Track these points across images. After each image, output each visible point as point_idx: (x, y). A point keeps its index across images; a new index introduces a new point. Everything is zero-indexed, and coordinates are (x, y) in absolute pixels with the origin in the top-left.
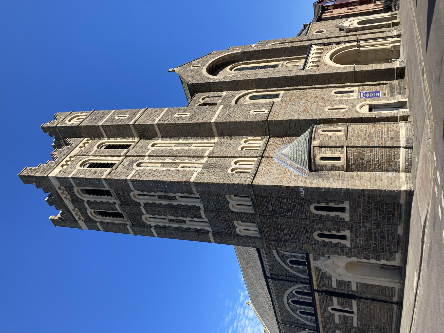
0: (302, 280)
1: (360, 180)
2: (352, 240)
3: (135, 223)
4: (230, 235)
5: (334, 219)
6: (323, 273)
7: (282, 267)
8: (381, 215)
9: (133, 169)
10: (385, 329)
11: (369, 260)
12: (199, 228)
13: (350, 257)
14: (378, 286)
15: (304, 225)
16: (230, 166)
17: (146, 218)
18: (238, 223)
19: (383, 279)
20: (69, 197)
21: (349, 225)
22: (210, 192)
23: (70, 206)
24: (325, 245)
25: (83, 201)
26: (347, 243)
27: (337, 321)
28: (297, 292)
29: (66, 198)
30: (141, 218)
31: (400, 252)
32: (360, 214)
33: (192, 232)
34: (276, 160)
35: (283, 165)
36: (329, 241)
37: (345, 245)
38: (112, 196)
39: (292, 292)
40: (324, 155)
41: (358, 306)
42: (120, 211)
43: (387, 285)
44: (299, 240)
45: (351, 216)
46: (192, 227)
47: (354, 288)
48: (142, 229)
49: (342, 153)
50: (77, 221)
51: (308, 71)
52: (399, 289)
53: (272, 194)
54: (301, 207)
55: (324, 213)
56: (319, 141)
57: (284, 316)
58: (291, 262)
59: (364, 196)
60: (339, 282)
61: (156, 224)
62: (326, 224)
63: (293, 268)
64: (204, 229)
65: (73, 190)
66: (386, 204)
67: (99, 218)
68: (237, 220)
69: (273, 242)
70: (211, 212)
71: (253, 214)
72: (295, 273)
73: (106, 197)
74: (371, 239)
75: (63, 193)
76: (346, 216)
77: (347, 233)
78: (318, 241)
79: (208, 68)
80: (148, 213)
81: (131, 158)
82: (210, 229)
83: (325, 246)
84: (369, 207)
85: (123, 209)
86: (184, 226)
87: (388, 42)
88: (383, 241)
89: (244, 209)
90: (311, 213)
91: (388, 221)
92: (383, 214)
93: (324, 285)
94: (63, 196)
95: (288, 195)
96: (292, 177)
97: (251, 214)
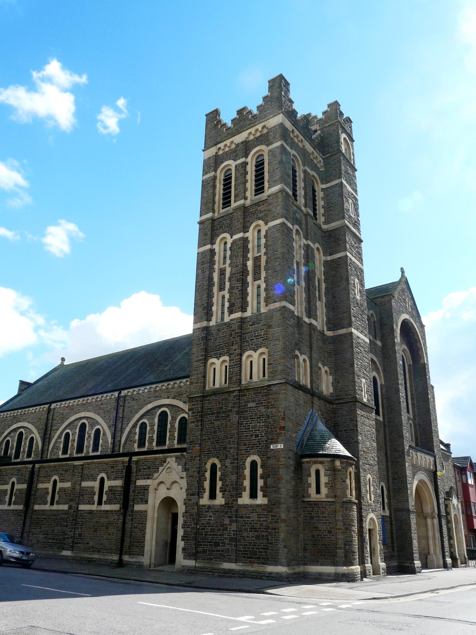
0: (119, 439)
1: (294, 517)
2: (209, 507)
3: (216, 223)
4: (206, 350)
6: (158, 468)
7: (137, 412)
8: (248, 543)
9: (293, 225)
10: (79, 545)
11: (182, 528)
12: (214, 308)
14: (144, 537)
15: (229, 446)
16: (301, 354)
17: (224, 238)
18: (224, 361)
20: (252, 137)
21: (232, 504)
22: (270, 327)
23: (239, 139)
24: (201, 472)
26: (205, 500)
27: (85, 484)
28: (98, 431)
30: (225, 232)
31: (197, 565)
32: (249, 517)
33: (208, 300)
34: (310, 413)
35: (305, 421)
36: (206, 478)
39: (98, 423)
40: (322, 473)
41: (111, 511)
42: (234, 205)
43: (147, 548)
44: (205, 440)
45: (245, 506)
46: (214, 300)
47: (138, 507)
48: (209, 233)
49: (327, 496)
50: (216, 145)
52: (143, 563)
53: (271, 408)
54: (254, 444)
55: (247, 472)
57: (61, 412)
58: (144, 424)
59: (276, 522)
60: (146, 488)
61: (217, 251)
62: (232, 474)
63: (134, 426)
64: (212, 316)
65: (262, 144)
66: (266, 549)
67: (220, 176)
68: (230, 361)
69: (200, 406)
70: (241, 327)
72: (128, 429)
73: (254, 188)
74: (212, 530)
75: (257, 130)
76: (245, 499)
77: (220, 500)
78: (206, 464)
79: (406, 321)
80: (233, 243)
81: (304, 222)
82: (213, 323)
83: (199, 472)
84: (259, 528)
85: (236, 209)
86: (215, 289)
88: (210, 545)
90: (247, 457)
91: (240, 551)
92: (250, 545)
93: (140, 470)
94: (252, 130)
95: (271, 428)
96: (295, 433)
97: (240, 380)
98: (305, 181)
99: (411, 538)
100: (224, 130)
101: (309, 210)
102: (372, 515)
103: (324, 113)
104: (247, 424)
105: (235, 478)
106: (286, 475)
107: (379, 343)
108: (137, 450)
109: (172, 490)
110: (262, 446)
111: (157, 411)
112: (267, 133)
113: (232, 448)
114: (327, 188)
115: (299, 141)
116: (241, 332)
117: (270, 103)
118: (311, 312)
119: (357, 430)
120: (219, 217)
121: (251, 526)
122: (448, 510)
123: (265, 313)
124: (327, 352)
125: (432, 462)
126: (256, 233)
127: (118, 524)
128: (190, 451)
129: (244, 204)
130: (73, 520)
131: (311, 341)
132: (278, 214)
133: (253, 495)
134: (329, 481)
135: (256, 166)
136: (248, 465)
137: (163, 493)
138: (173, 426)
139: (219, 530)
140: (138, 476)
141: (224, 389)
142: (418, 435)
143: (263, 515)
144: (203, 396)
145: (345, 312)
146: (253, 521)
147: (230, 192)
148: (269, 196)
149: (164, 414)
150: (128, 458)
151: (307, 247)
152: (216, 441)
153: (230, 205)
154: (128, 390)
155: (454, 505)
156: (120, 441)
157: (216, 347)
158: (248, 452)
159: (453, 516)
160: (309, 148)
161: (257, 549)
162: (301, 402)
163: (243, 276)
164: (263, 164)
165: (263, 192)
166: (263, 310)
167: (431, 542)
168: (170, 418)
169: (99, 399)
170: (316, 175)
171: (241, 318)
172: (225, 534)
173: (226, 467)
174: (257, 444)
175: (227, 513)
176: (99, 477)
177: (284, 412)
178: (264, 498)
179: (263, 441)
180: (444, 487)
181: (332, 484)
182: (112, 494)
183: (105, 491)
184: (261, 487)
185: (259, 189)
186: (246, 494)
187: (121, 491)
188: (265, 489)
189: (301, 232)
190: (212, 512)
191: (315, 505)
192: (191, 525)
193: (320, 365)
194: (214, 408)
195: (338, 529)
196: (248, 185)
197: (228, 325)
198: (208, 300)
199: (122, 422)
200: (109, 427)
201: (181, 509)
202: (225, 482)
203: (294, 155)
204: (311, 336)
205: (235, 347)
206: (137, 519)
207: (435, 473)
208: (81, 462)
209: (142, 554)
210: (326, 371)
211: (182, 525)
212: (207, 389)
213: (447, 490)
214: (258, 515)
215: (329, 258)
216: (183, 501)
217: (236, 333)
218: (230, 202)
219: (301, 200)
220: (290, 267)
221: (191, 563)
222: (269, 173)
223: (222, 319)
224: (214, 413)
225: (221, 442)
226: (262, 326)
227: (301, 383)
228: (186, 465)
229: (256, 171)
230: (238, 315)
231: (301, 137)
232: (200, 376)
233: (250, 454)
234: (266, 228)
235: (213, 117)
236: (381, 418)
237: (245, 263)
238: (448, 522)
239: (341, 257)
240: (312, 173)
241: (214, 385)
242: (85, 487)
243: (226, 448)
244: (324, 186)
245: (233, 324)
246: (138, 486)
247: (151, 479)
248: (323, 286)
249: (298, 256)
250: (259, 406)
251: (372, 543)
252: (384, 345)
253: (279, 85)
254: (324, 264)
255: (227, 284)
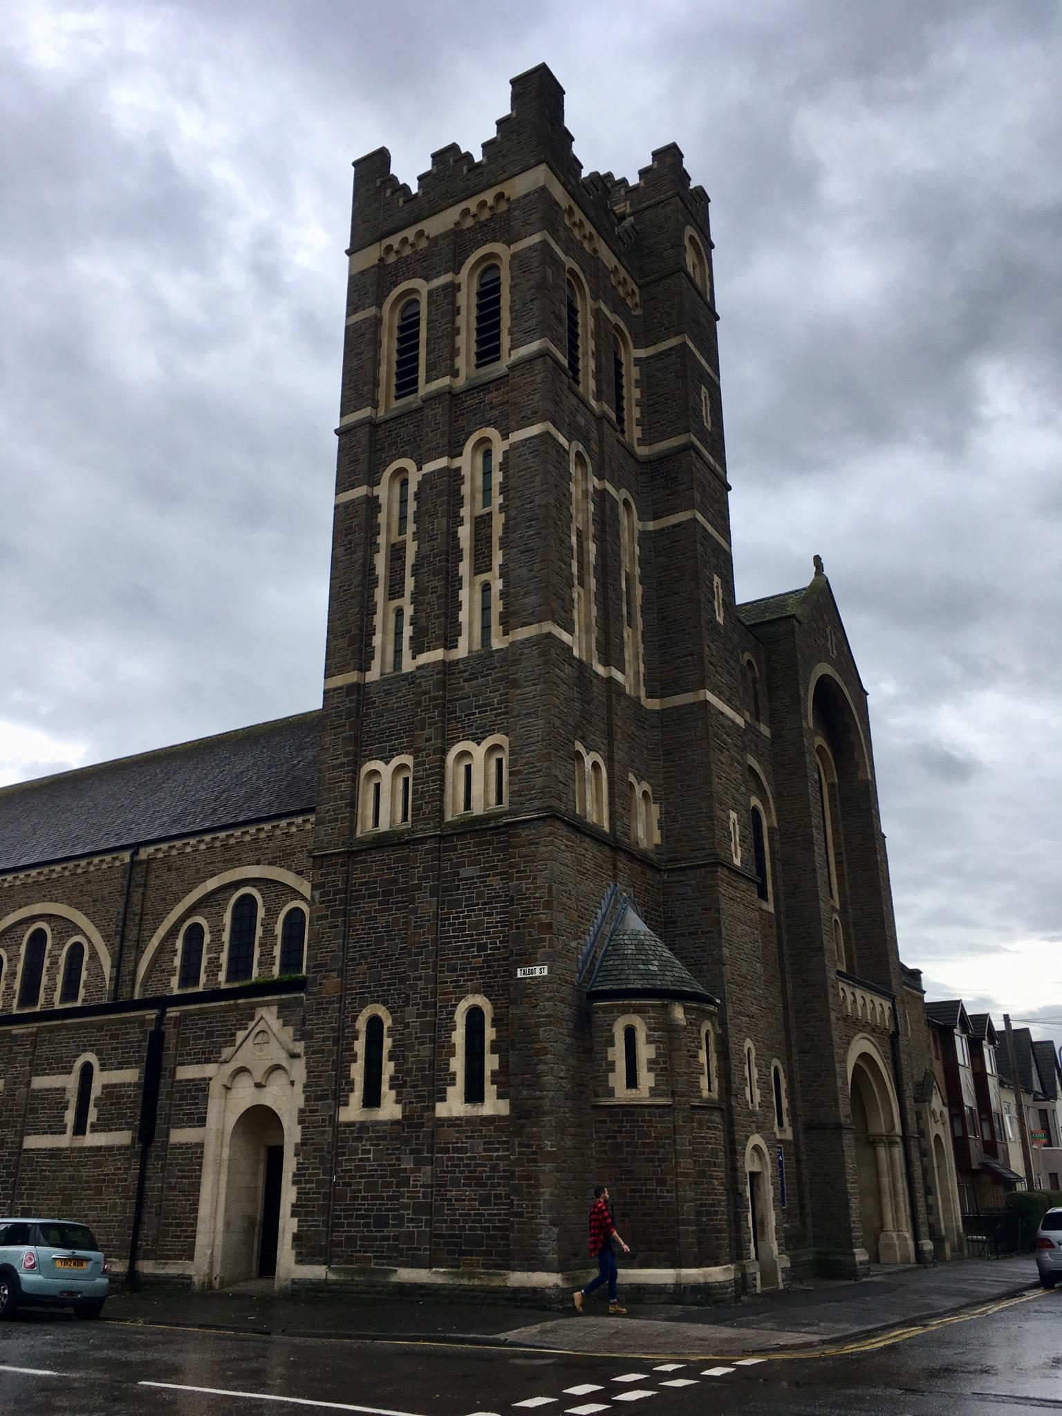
2: (363, 1127)
3: (381, 433)
4: (357, 741)
5: (441, 1070)
6: (234, 1035)
7: (178, 900)
9: (570, 441)
11: (294, 1183)
12: (377, 640)
13: (300, 1122)
14: (196, 1211)
16: (589, 749)
17: (402, 470)
18: (403, 767)
19: (220, 1225)
21: (421, 1117)
23: (437, 225)
24: (344, 1039)
25: (457, 271)
26: (353, 1111)
28: (77, 950)
29: (466, 212)
30: (404, 455)
31: (332, 1277)
33: (362, 620)
36: (356, 1055)
37: (346, 1104)
38: (478, 366)
39: (77, 930)
40: (641, 1036)
42: (424, 389)
43: (202, 1239)
44: (353, 960)
45: (453, 1122)
46: (378, 619)
47: (179, 1136)
48: (364, 457)
49: (653, 1092)
50: (380, 239)
51: (835, 987)
52: (190, 1277)
53: (519, 879)
55: (459, 1037)
56: (684, 1023)
58: (197, 928)
60: (201, 1086)
61: (383, 500)
62: (422, 1043)
63: (172, 933)
64: (373, 658)
65: (495, 240)
66: (506, 1228)
67: (391, 319)
70: (442, 685)
71: (442, 818)
72: (155, 942)
73: (474, 347)
74: (371, 1187)
75: (483, 204)
76: (453, 1105)
78: (355, 1019)
81: (594, 435)
83: (337, 1041)
84: (488, 1178)
86: (380, 594)
87: (904, 1228)
88: (365, 1225)
89: (454, 788)
90: (459, 999)
92: (465, 1222)
93: (185, 1042)
94: (472, 204)
97: (441, 811)
98: (597, 336)
99: (845, 1192)
100: (401, 203)
101: (606, 407)
102: (756, 1139)
103: (643, 173)
104: (458, 918)
105: (428, 1053)
106: (554, 1039)
107: (765, 730)
108: (176, 992)
109: (266, 1089)
110: (495, 972)
111: (231, 895)
112: (508, 211)
113: (420, 978)
114: (648, 358)
115: (585, 237)
116: (444, 697)
117: (514, 137)
118: (610, 652)
119: (720, 932)
120: (389, 415)
121: (469, 1172)
122: (922, 1126)
123: (501, 650)
124: (647, 748)
125: (887, 1012)
126: (479, 460)
127: (126, 1180)
128: (316, 989)
129: (450, 387)
130: (8, 1175)
131: (610, 718)
132: (535, 413)
133: (474, 1094)
134: (658, 1055)
135: (480, 295)
136: (460, 1018)
137: (244, 1096)
138: (269, 931)
139: (388, 1185)
140: (182, 1055)
141: (402, 833)
142: (854, 948)
143: (499, 1143)
144: (351, 854)
145: (691, 655)
146: (474, 1158)
147: (416, 358)
148: (512, 368)
149: (247, 903)
150: (156, 1011)
151: (602, 495)
152: (381, 961)
153: (416, 391)
154: (158, 847)
155: (933, 1113)
156: (134, 972)
157: (382, 732)
158: (461, 986)
159: (932, 1139)
160: (608, 258)
161: (483, 1229)
162: (589, 865)
163: (448, 561)
164: (497, 289)
165: (498, 359)
166: (497, 643)
167: (887, 1202)
168: (261, 913)
169: (79, 871)
170: (622, 325)
171: (443, 662)
172: (402, 1195)
173: (407, 1025)
174: (482, 968)
175: (406, 1141)
176: (78, 1064)
177: (550, 888)
178: (501, 1101)
179: (498, 960)
180: (913, 1072)
181: (665, 1062)
182: (112, 1104)
183: (93, 1097)
184: (493, 1073)
185: (488, 350)
186: (456, 1092)
187: (135, 1096)
188: (502, 1079)
189: (588, 460)
190: (369, 1139)
191: (624, 1115)
192: (318, 1174)
193: (632, 778)
194: (375, 882)
195: (682, 1175)
196: (461, 340)
197: (411, 678)
198: (362, 620)
199: (140, 925)
200: (106, 938)
201: (292, 1134)
202: (402, 1064)
203: (571, 271)
204: (610, 710)
205: (429, 732)
206: (177, 1164)
207: (894, 1037)
208: (33, 1027)
209: (188, 1253)
210: (645, 794)
211: (294, 1175)
212: (359, 834)
213: (919, 1077)
214: (485, 1143)
215: (651, 526)
216: (295, 1114)
217: (430, 699)
218: (415, 382)
219: (589, 385)
220: (563, 542)
221: (317, 1272)
222: (512, 310)
223: (397, 663)
224: (377, 894)
225: (393, 965)
226: (494, 681)
227: (588, 820)
228: (304, 1024)
229: (480, 307)
230: (435, 655)
231: (589, 228)
232: (342, 803)
233: (467, 992)
234: (505, 445)
235: (373, 171)
236: (770, 907)
237: (452, 530)
238: (924, 1153)
239: (680, 524)
240: (615, 319)
241: (376, 824)
242: (40, 1091)
243: (407, 978)
244: (641, 353)
245: (423, 677)
246: (181, 1081)
247: (216, 1062)
248: (639, 590)
249: (580, 517)
250: (488, 876)
251: (759, 1206)
252: (776, 736)
253: (538, 95)
254: (639, 538)
255: (410, 583)
